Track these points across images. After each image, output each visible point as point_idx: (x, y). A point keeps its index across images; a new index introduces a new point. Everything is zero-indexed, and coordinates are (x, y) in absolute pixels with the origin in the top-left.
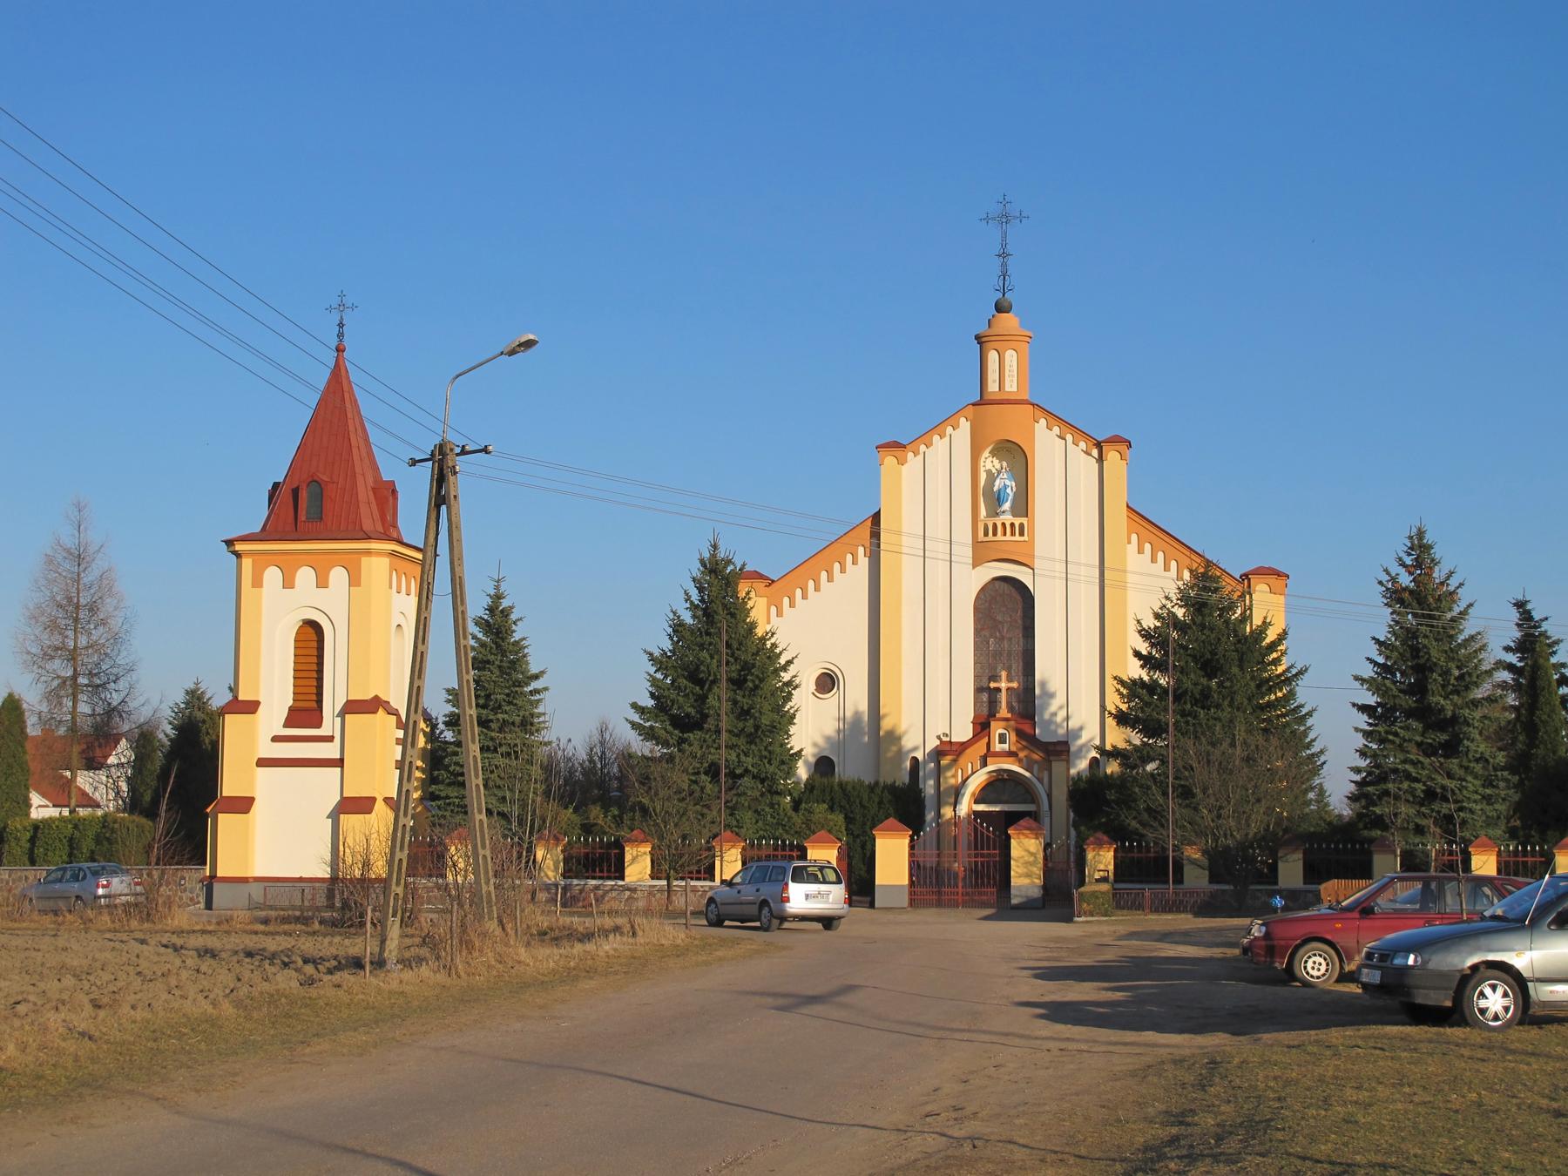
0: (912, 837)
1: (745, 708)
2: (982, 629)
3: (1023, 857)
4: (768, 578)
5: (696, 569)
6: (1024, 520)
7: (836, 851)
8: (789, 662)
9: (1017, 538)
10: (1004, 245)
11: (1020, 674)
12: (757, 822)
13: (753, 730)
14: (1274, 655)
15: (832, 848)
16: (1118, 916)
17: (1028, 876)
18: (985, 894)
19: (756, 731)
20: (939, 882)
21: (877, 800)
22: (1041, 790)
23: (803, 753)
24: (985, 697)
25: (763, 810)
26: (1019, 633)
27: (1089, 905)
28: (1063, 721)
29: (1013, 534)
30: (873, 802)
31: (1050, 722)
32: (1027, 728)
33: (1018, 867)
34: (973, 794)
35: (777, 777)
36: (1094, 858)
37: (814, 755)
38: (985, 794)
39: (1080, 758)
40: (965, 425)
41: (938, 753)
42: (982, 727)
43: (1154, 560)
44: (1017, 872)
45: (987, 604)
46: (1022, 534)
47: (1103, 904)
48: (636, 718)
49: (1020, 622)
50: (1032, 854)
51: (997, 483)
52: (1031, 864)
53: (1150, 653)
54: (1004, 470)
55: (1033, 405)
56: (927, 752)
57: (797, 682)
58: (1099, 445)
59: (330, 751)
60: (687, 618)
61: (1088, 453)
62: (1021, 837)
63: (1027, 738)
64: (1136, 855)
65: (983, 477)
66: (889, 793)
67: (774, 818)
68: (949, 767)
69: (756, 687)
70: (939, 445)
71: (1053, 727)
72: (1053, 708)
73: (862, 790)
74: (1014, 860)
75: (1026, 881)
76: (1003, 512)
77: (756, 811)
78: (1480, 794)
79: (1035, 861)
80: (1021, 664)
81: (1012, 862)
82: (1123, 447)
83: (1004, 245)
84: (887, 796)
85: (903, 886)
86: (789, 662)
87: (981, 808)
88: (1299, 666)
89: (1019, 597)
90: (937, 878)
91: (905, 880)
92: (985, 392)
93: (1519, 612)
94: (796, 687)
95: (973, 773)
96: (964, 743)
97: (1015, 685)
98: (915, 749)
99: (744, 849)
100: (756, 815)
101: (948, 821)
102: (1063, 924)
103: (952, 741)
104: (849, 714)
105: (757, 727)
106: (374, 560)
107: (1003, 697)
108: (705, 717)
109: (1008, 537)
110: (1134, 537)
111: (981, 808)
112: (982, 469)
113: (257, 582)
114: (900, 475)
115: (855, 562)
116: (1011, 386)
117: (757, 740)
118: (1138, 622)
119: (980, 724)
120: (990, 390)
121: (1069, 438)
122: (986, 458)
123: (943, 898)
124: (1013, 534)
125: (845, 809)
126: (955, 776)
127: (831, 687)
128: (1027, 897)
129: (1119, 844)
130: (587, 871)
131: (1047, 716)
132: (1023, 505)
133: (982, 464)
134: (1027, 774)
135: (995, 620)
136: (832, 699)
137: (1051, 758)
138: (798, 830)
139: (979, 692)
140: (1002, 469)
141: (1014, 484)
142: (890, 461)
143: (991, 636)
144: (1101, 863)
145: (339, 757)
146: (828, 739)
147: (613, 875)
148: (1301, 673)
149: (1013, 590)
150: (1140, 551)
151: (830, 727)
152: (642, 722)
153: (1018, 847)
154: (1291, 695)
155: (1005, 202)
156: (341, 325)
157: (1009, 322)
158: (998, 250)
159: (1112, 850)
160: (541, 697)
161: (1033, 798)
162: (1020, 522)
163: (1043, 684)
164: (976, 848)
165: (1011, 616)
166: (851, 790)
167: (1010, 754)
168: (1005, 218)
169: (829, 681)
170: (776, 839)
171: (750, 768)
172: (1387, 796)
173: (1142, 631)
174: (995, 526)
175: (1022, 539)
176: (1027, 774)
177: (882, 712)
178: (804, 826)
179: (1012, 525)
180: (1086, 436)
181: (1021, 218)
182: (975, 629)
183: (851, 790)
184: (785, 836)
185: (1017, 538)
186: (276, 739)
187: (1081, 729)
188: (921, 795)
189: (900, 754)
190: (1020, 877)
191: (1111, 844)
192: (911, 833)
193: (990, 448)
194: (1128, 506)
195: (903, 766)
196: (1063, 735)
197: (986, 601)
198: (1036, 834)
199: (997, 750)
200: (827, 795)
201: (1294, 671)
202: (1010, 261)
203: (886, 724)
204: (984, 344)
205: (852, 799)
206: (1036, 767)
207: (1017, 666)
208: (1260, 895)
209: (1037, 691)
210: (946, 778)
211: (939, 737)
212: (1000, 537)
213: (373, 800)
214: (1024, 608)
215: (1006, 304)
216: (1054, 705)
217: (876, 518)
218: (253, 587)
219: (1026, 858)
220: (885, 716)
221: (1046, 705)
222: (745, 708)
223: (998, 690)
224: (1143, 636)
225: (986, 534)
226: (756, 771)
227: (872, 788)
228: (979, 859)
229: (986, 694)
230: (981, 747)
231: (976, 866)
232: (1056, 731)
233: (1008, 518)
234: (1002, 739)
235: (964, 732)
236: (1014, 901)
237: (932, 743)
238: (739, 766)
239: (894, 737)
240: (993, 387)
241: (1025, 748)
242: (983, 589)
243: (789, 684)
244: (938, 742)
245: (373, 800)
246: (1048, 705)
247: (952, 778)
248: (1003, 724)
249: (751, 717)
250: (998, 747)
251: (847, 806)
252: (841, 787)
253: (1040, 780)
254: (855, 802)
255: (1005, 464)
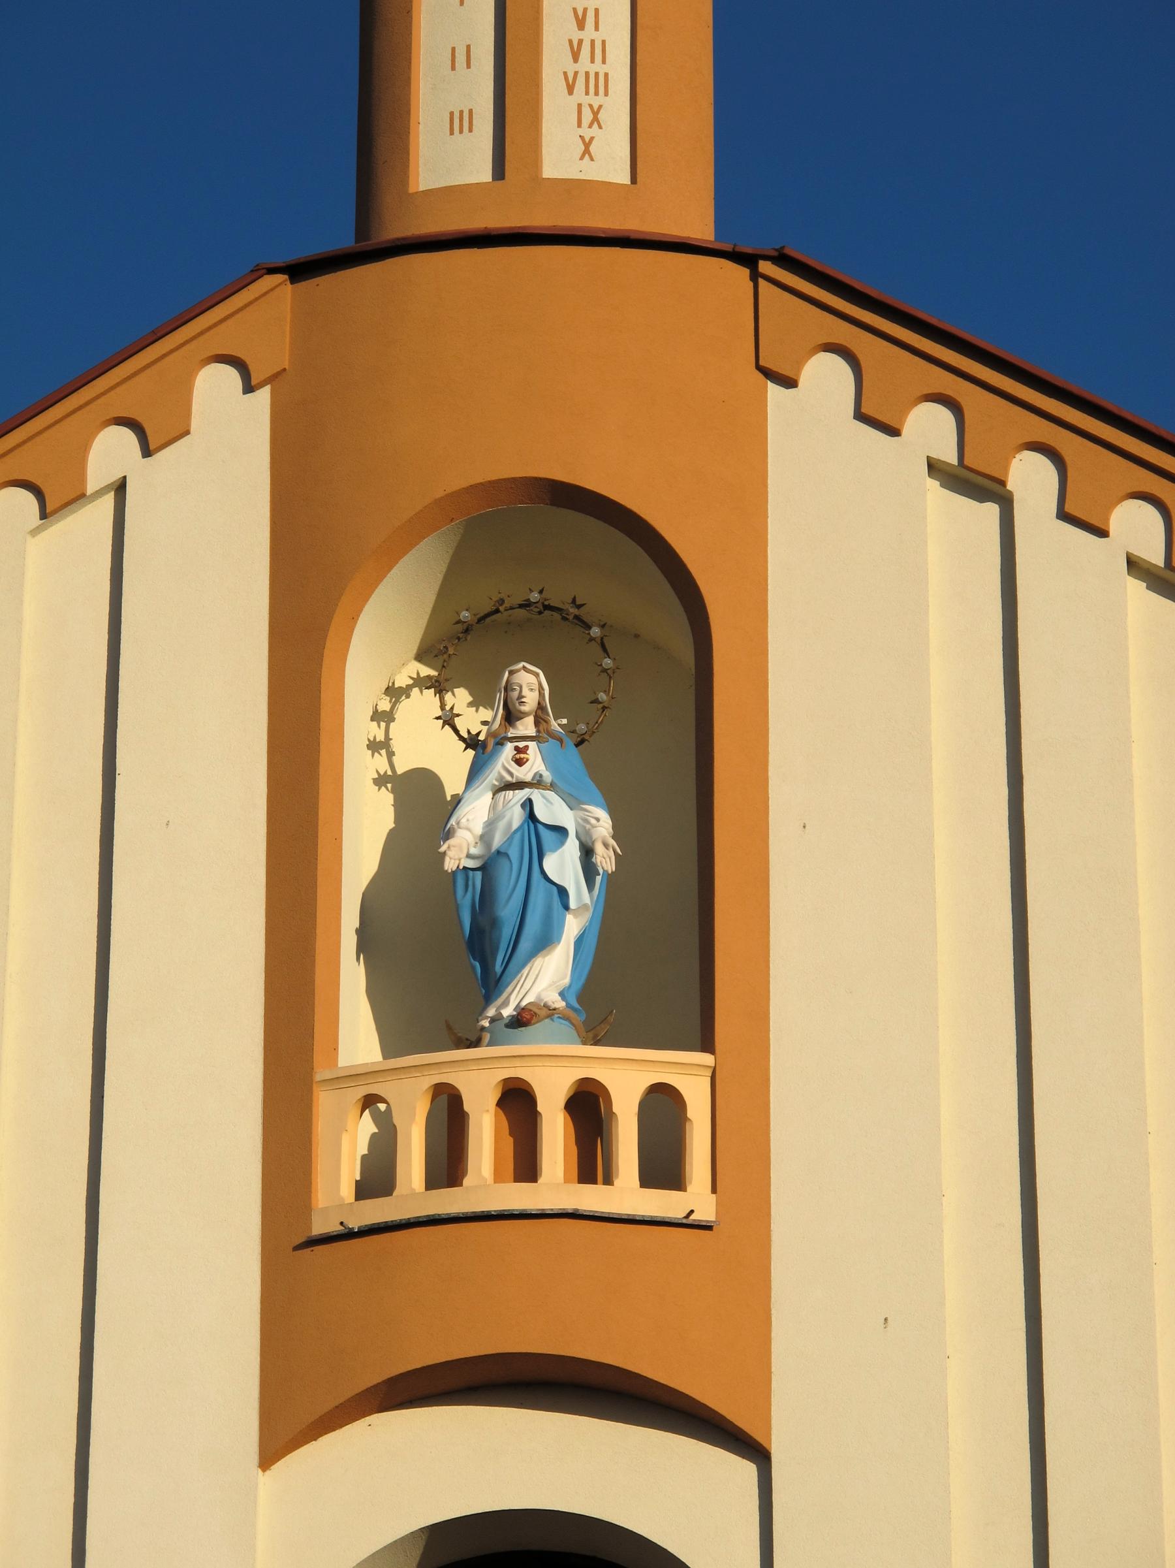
54: (526, 727)
55: (748, 260)
122: (395, 693)
140: (511, 717)
141: (602, 823)
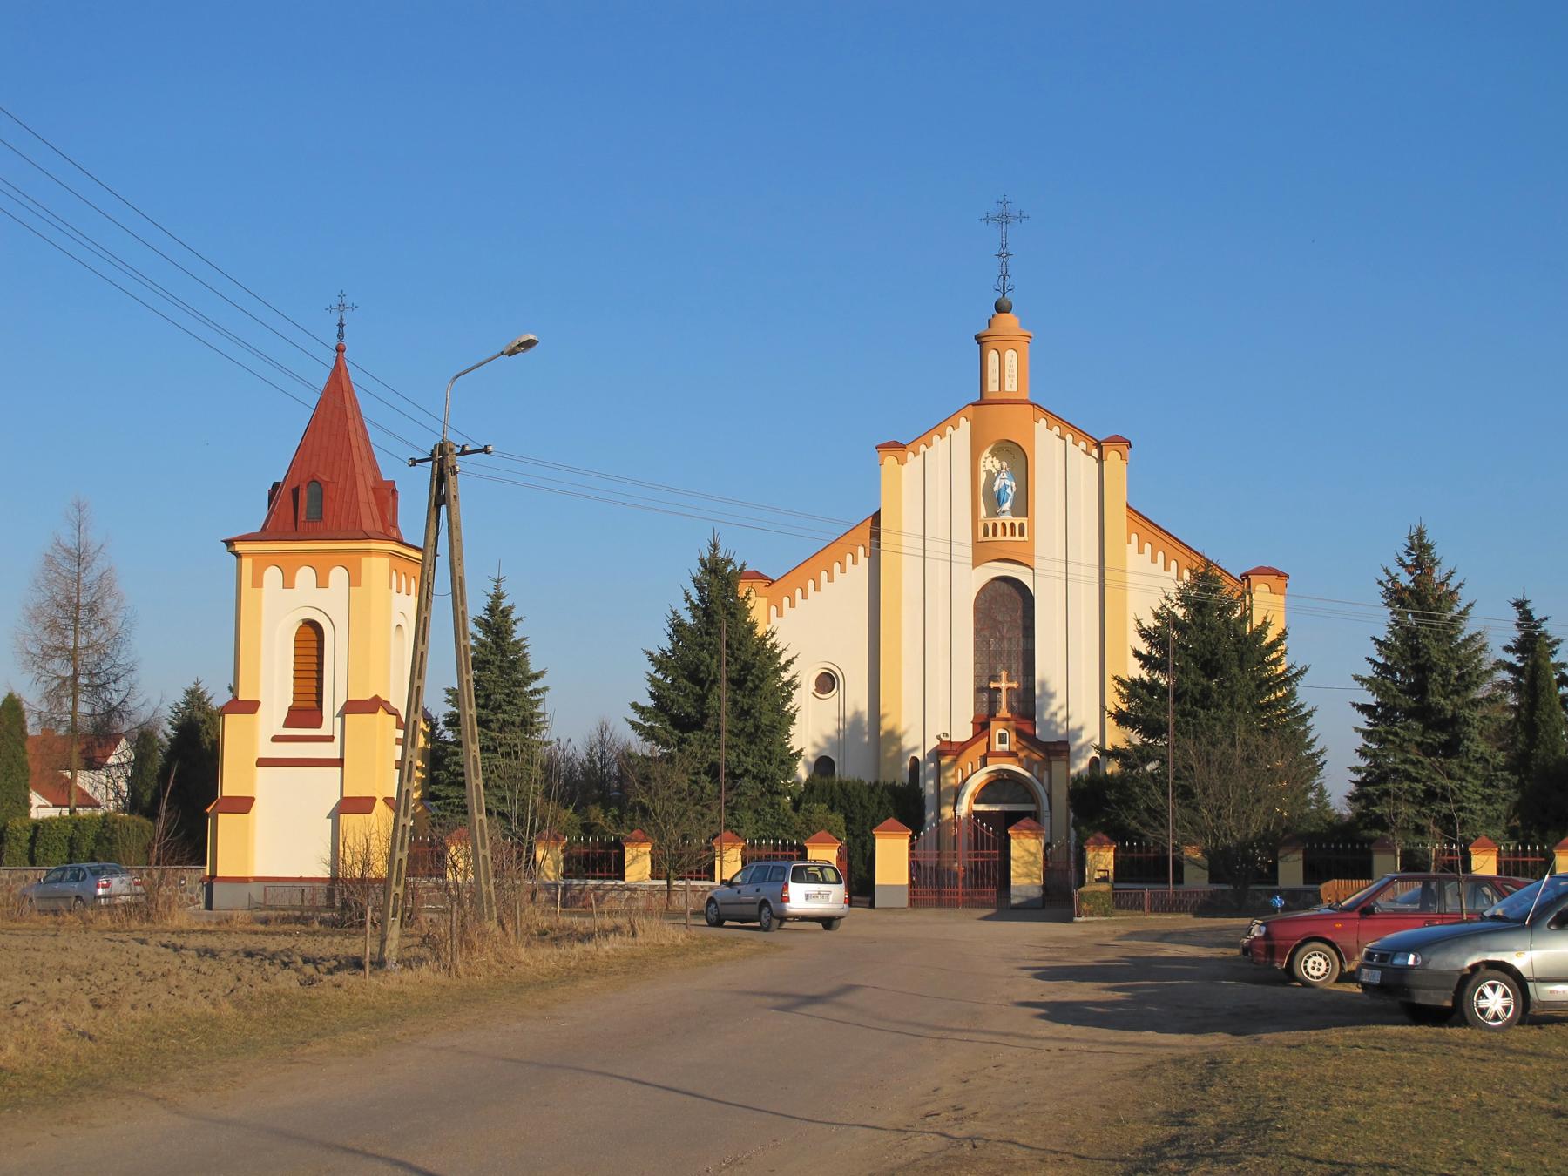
0: (912, 837)
1: (745, 708)
2: (982, 629)
3: (1023, 857)
4: (768, 578)
5: (696, 569)
6: (1024, 520)
7: (836, 851)
8: (789, 662)
9: (1017, 538)
10: (1004, 245)
11: (1020, 674)
12: (757, 822)
13: (753, 730)
14: (1274, 655)
15: (832, 848)
16: (1118, 916)
17: (1028, 876)
18: (985, 894)
19: (756, 731)
20: (939, 882)
21: (877, 800)
22: (1041, 790)
23: (803, 753)
24: (985, 697)
25: (763, 810)
26: (1019, 633)
27: (1089, 905)
28: (1063, 721)
29: (1013, 534)
30: (873, 802)
31: (1050, 722)
32: (1027, 728)
33: (1018, 867)
34: (973, 794)
35: (777, 777)
36: (1094, 858)
37: (814, 755)
38: (985, 794)
39: (1080, 758)
40: (965, 425)
41: (938, 753)
42: (982, 727)
43: (1154, 560)
44: (1017, 872)
45: (987, 604)
46: (1022, 534)
47: (1103, 904)
48: (636, 718)
49: (1020, 622)
50: (1032, 854)
51: (997, 483)
52: (1031, 864)
53: (1150, 653)
54: (1004, 470)
55: (1033, 405)
56: (927, 752)
57: (797, 682)
58: (1099, 445)
59: (330, 751)
60: (687, 618)
61: (1088, 453)
62: (1021, 837)
63: (1027, 738)
64: (1136, 855)
65: (983, 477)
66: (889, 793)
67: (774, 818)
68: (949, 767)
69: (756, 687)
70: (939, 445)
71: (1053, 727)
72: (1053, 708)
73: (862, 790)
74: (1014, 860)
75: (1026, 881)
76: (1003, 512)
77: (756, 811)
78: (1480, 794)
79: (1035, 861)
80: (1021, 664)
81: (1012, 862)
82: (1123, 447)
83: (1004, 245)
84: (887, 796)
85: (903, 886)
86: (789, 662)
87: (981, 808)
88: (1299, 666)
89: (1019, 597)
90: (937, 878)
91: (905, 880)
92: (985, 392)
93: (1519, 612)
94: (796, 687)
95: (973, 773)
96: (964, 743)
97: (1015, 685)
98: (915, 749)
99: (744, 849)
100: (756, 815)
101: (948, 821)
102: (1063, 924)
103: (952, 741)
104: (849, 714)
105: (757, 727)
106: (374, 560)
107: (1003, 697)
108: (705, 717)
109: (1008, 537)
110: (1134, 537)
111: (981, 808)
112: (982, 469)
113: (257, 582)
114: (900, 475)
115: (855, 562)
116: (1011, 386)
117: (757, 740)
118: (1138, 622)
119: (980, 724)
120: (990, 390)
121: (1069, 438)
122: (986, 458)
123: (943, 898)
124: (1013, 534)
125: (845, 809)
126: (955, 776)
127: (831, 687)
128: (1027, 897)
129: (1119, 844)
130: (587, 871)
131: (1047, 716)
132: (1023, 505)
133: (982, 464)
134: (1027, 774)
135: (995, 620)
136: (832, 699)
137: (1051, 758)
138: (798, 830)
139: (979, 692)
140: (1002, 469)
141: (1014, 484)
142: (890, 461)
143: (991, 636)
144: (1101, 863)
145: (339, 757)
146: (828, 739)
147: (613, 875)
148: (1301, 673)
149: (1013, 590)
150: (1140, 551)
151: (830, 727)
152: (642, 722)
153: (1018, 847)
154: (1291, 695)
155: (1005, 202)
156: (341, 325)
157: (1009, 322)
158: (998, 250)
159: (1112, 850)
160: (541, 697)
161: (1033, 798)
162: (1020, 522)
163: (1043, 684)
164: (976, 848)
165: (1011, 616)
166: (851, 790)
167: (1010, 754)
168: (1005, 218)
169: (829, 681)
170: (776, 839)
171: (750, 768)
172: (1387, 796)
173: (1142, 631)
174: (995, 526)
175: (1022, 539)
176: (1027, 774)
177: (882, 712)
178: (804, 826)
179: (1012, 525)
180: (1086, 436)
181: (1021, 218)
182: (975, 629)
183: (851, 790)
184: (785, 836)
185: (1017, 538)
186: (276, 739)
187: (1081, 729)
188: (921, 795)
189: (900, 754)
190: (1020, 877)
191: (1111, 844)
192: (911, 833)
193: (990, 448)
194: (1128, 506)
195: (903, 766)
196: (1063, 735)
197: (986, 601)
198: (1036, 834)
199: (997, 750)
200: (827, 795)
201: (1294, 671)
202: (1010, 261)
203: (886, 724)
204: (984, 344)
205: (852, 799)
206: (1036, 767)
207: (1017, 666)
208: (1260, 895)
209: (1037, 691)
210: (946, 778)
211: (939, 737)
212: (1000, 537)
213: (373, 800)
214: (1024, 608)
215: (1006, 304)
216: (1054, 705)
217: (876, 518)
218: (253, 587)
219: (1026, 858)
220: (885, 716)
221: (1046, 705)
222: (745, 708)
223: (998, 690)
224: (1143, 636)
225: (986, 534)
226: (756, 771)
227: (872, 788)
228: (979, 859)
229: (986, 694)
230: (981, 747)
231: (976, 866)
232: (1056, 731)
233: (1008, 518)
234: (1002, 739)
235: (964, 732)
236: (1014, 901)
237: (932, 743)
238: (739, 766)
239: (894, 737)
240: (993, 387)
241: (1025, 748)
242: (983, 589)
243: (789, 684)
244: (938, 742)
245: (373, 800)
246: (1048, 705)
247: (952, 778)
248: (1003, 724)
249: (751, 717)
250: (998, 747)
251: (847, 806)
252: (841, 787)
253: (1040, 780)
254: (855, 802)
255: (1005, 464)
